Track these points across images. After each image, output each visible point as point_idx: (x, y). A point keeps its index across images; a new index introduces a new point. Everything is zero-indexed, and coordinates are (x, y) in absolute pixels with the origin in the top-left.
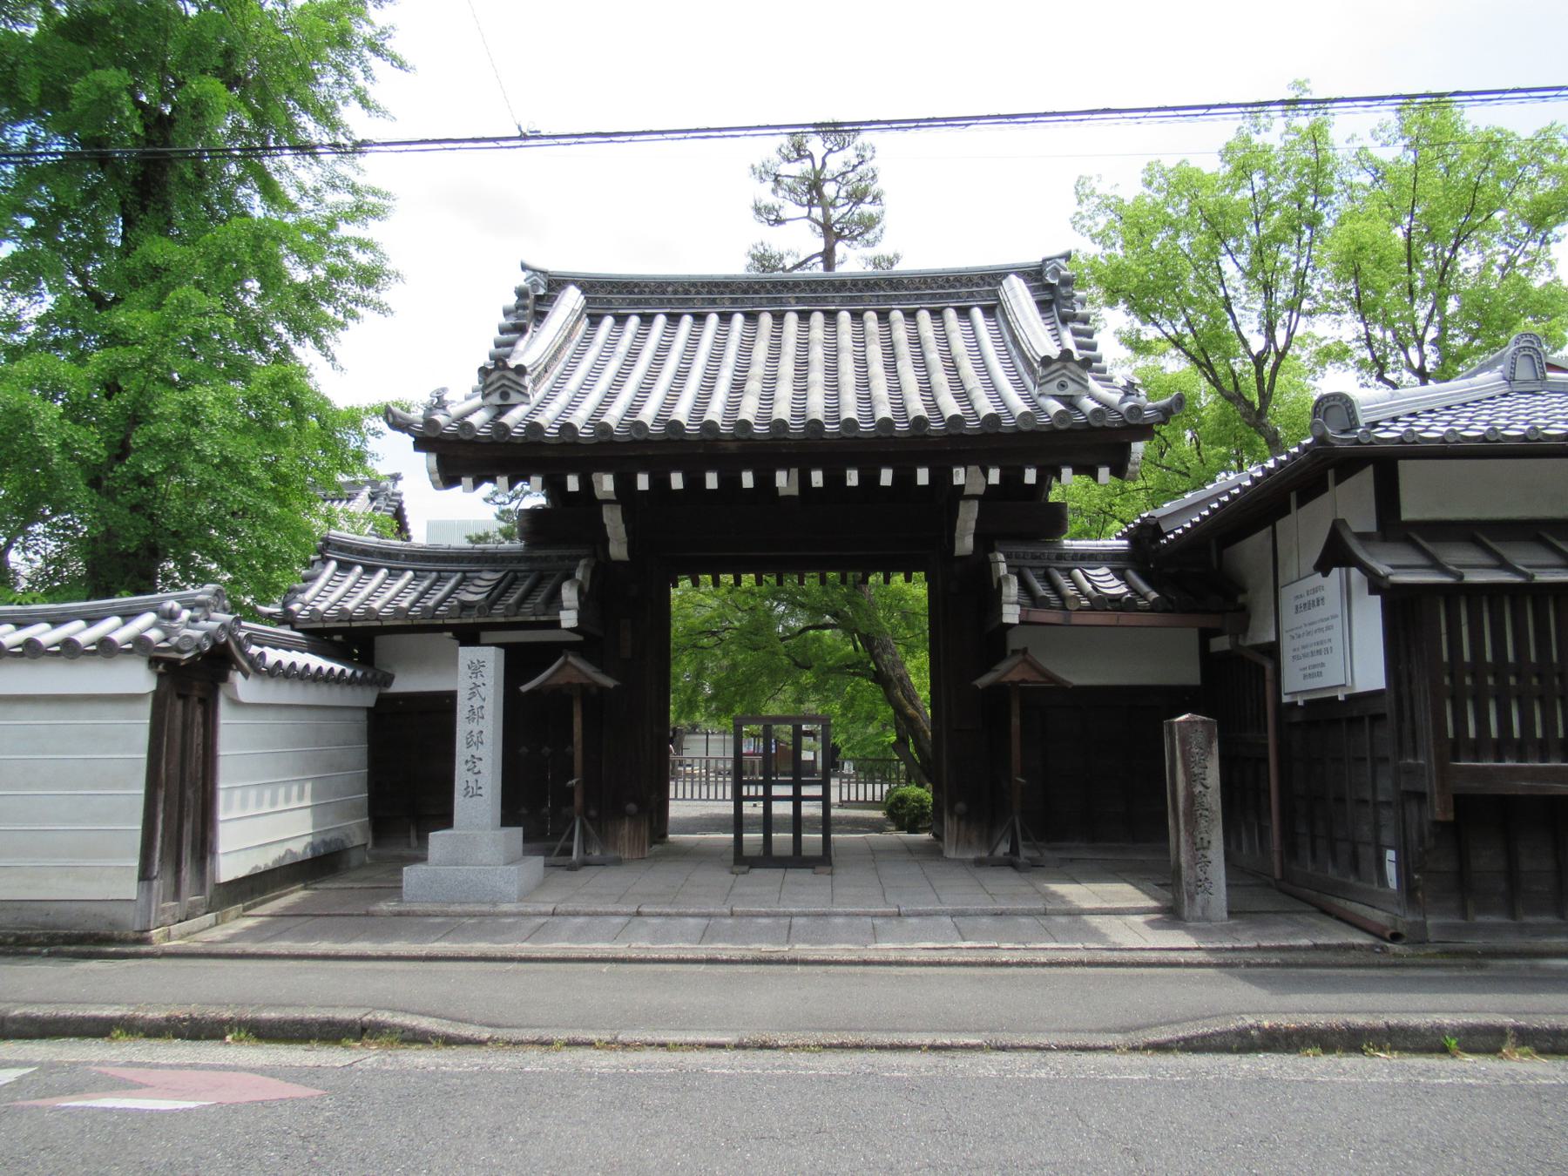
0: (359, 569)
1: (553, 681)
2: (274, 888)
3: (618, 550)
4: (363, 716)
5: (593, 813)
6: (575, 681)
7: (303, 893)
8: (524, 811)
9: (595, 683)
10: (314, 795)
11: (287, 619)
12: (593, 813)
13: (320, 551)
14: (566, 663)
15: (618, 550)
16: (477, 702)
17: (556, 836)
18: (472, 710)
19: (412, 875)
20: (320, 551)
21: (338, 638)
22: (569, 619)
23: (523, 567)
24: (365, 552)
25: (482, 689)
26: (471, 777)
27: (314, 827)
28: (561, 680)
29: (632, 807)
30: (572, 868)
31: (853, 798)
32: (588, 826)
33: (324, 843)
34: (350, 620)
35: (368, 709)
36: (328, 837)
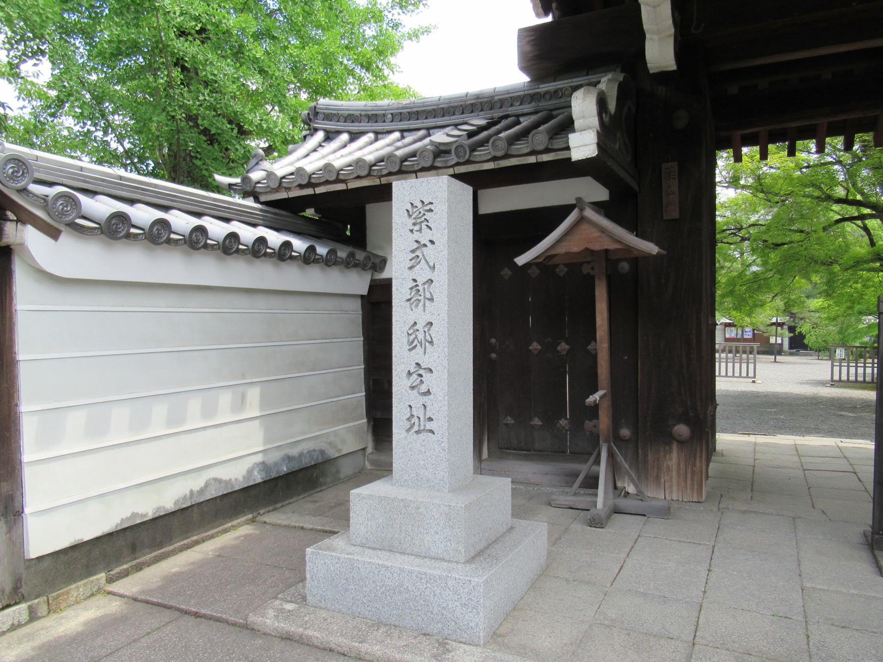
0: (345, 137)
1: (561, 250)
2: (186, 532)
3: (660, 53)
4: (357, 304)
5: (625, 432)
6: (597, 247)
7: (246, 530)
8: (537, 422)
9: (629, 249)
10: (263, 404)
11: (250, 192)
12: (625, 432)
13: (308, 121)
14: (581, 220)
15: (660, 53)
16: (422, 273)
17: (581, 455)
18: (415, 288)
19: (322, 560)
20: (308, 121)
21: (310, 212)
22: (583, 145)
23: (527, 108)
24: (351, 118)
25: (429, 251)
26: (417, 401)
27: (266, 441)
28: (575, 246)
29: (682, 430)
30: (596, 523)
31: (844, 378)
32: (620, 458)
33: (289, 458)
34: (310, 185)
35: (362, 297)
36: (294, 452)
